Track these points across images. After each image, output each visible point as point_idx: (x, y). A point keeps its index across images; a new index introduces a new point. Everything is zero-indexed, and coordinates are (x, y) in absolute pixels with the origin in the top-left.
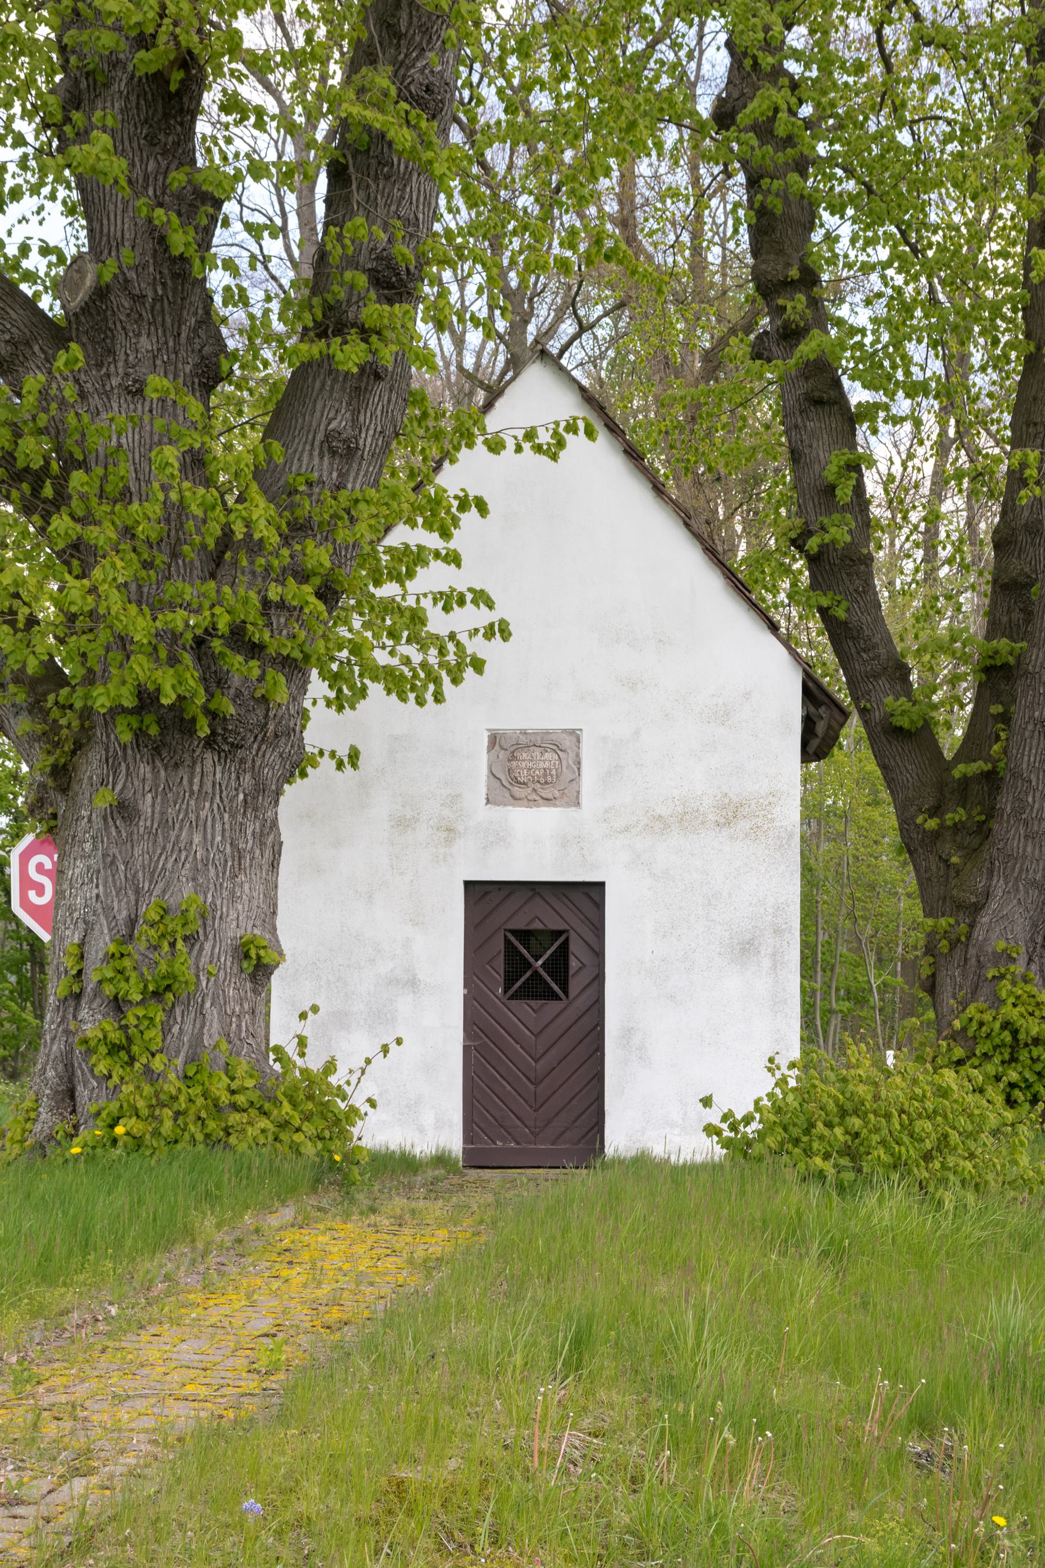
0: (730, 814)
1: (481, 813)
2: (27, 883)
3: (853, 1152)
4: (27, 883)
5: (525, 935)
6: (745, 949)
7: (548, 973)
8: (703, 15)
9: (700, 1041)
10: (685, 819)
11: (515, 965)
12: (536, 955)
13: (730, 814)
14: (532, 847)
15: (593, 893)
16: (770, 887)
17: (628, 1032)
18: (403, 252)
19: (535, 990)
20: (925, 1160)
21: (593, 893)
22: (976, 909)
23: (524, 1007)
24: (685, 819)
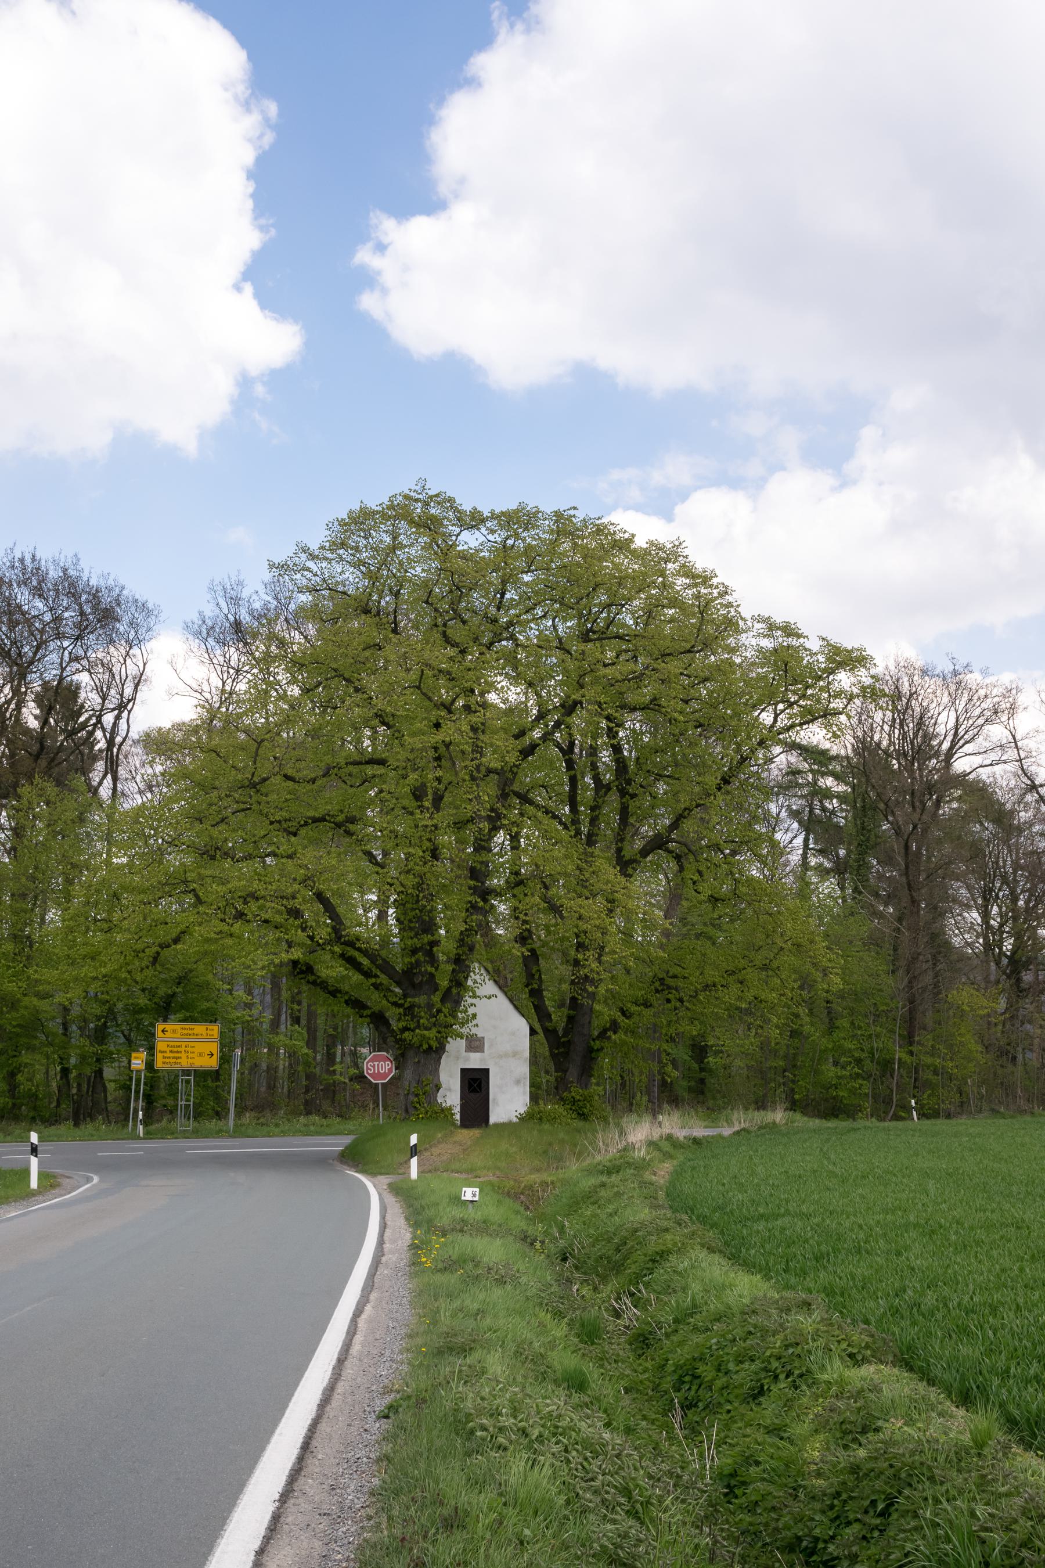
0: (515, 1054)
1: (464, 1054)
2: (368, 1069)
3: (541, 1119)
4: (368, 1069)
5: (472, 1079)
6: (518, 1082)
7: (39, 1173)
8: (946, 898)
9: (509, 1101)
10: (506, 1055)
11: (470, 1085)
12: (476, 1083)
13: (515, 1054)
14: (474, 1061)
15: (487, 1071)
16: (523, 1069)
17: (524, 1093)
18: (285, 970)
19: (474, 1091)
20: (553, 1119)
21: (487, 1071)
22: (566, 1071)
23: (472, 1094)
24: (506, 1055)
